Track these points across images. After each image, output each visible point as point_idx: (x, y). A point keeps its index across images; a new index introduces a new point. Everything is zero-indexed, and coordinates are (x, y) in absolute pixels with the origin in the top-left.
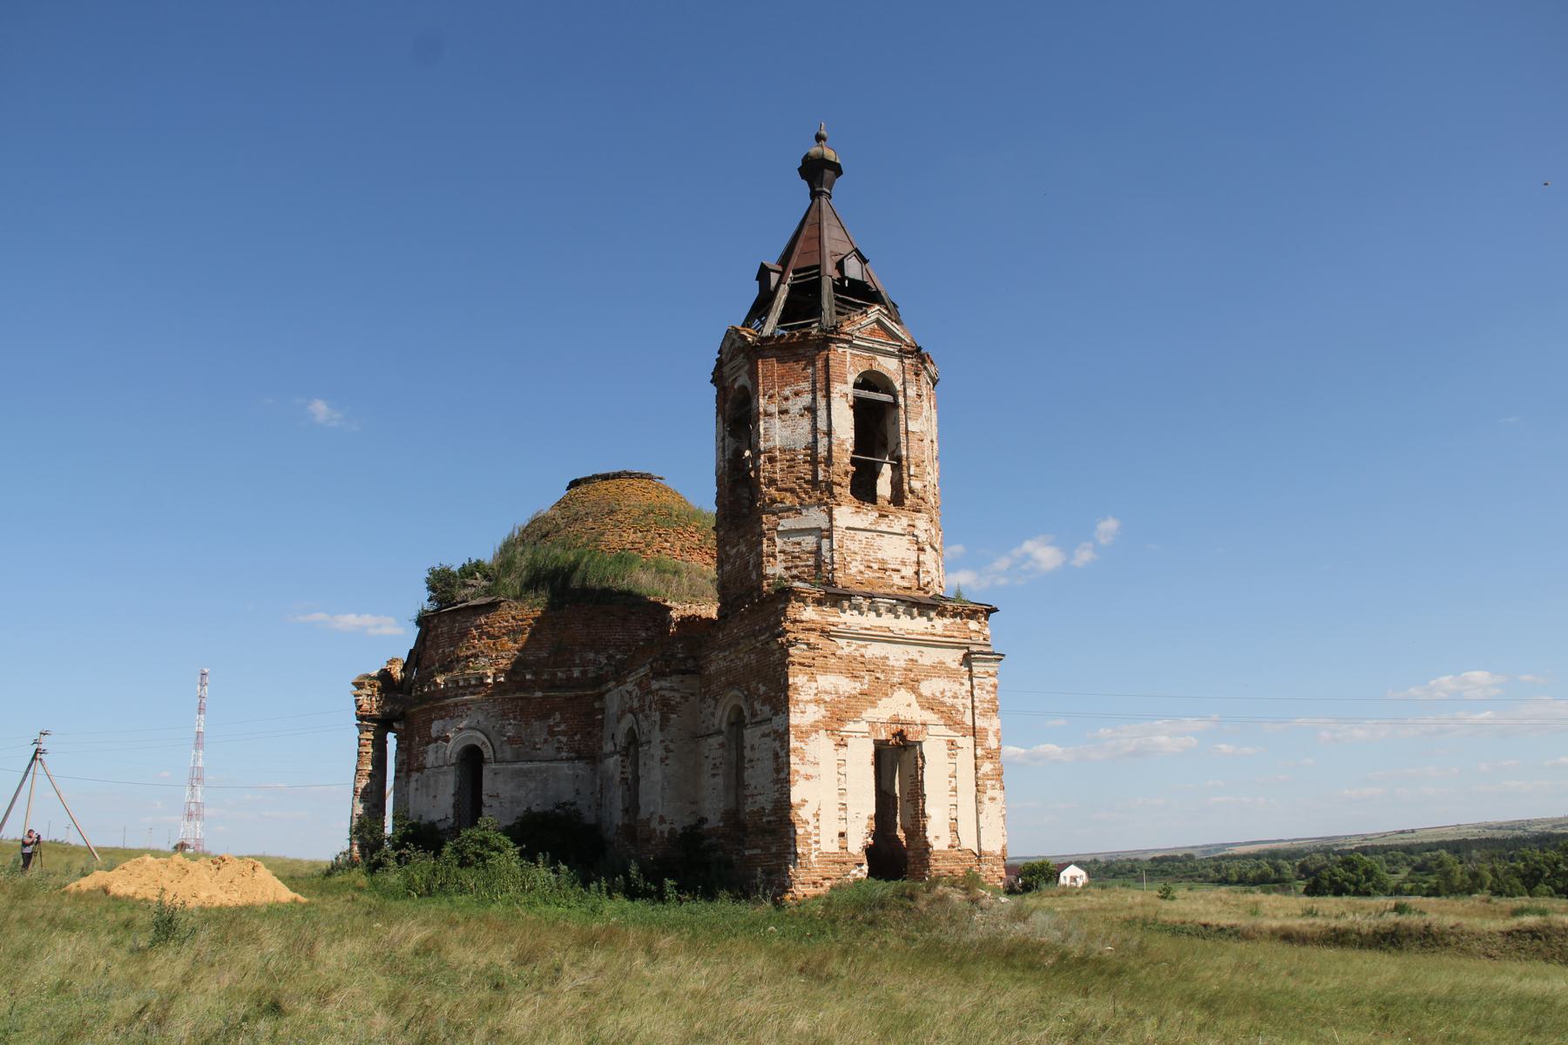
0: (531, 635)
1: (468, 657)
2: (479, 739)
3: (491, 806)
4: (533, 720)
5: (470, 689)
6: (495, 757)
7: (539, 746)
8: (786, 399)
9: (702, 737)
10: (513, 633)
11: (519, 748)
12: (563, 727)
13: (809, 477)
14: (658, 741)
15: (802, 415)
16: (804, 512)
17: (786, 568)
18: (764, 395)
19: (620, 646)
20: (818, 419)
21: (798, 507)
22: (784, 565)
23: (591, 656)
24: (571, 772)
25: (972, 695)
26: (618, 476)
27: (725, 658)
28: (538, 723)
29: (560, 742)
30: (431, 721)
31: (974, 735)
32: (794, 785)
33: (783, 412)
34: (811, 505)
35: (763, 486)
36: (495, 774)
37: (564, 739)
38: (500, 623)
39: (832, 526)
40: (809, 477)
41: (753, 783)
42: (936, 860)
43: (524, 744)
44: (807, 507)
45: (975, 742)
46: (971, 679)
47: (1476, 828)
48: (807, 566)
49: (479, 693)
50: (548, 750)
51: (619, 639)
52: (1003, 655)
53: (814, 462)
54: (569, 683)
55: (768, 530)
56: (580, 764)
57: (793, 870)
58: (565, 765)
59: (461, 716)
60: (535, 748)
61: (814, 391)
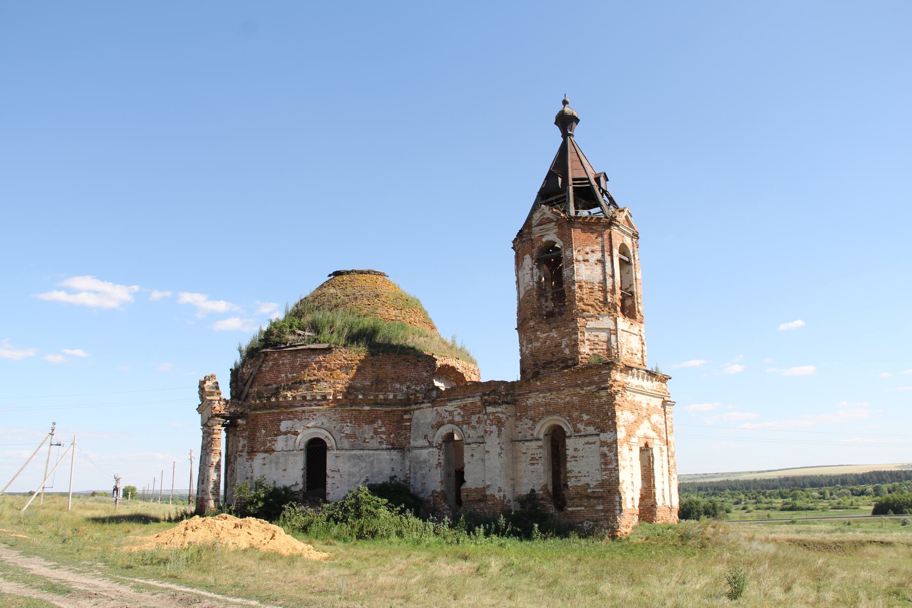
0: (359, 370)
1: (311, 381)
2: (322, 434)
3: (334, 477)
4: (363, 424)
5: (315, 402)
6: (337, 446)
7: (367, 440)
8: (587, 253)
9: (520, 441)
10: (345, 368)
11: (354, 441)
12: (383, 429)
13: (601, 299)
14: (497, 443)
15: (596, 264)
16: (601, 319)
18: (575, 250)
19: (413, 381)
20: (606, 267)
21: (598, 316)
22: (589, 347)
23: (398, 386)
24: (388, 457)
25: (666, 423)
26: (369, 272)
27: (544, 397)
28: (367, 426)
29: (381, 438)
30: (281, 421)
31: (667, 445)
33: (586, 261)
34: (605, 315)
35: (576, 301)
36: (337, 457)
37: (384, 437)
38: (334, 361)
39: (616, 329)
40: (601, 299)
41: (576, 470)
42: (658, 511)
43: (358, 438)
44: (603, 316)
45: (668, 448)
46: (665, 415)
48: (602, 349)
49: (322, 405)
50: (374, 443)
51: (412, 376)
52: (675, 402)
53: (604, 290)
54: (386, 402)
55: (580, 327)
56: (394, 452)
57: (619, 519)
58: (385, 453)
59: (308, 419)
60: (364, 442)
61: (603, 251)
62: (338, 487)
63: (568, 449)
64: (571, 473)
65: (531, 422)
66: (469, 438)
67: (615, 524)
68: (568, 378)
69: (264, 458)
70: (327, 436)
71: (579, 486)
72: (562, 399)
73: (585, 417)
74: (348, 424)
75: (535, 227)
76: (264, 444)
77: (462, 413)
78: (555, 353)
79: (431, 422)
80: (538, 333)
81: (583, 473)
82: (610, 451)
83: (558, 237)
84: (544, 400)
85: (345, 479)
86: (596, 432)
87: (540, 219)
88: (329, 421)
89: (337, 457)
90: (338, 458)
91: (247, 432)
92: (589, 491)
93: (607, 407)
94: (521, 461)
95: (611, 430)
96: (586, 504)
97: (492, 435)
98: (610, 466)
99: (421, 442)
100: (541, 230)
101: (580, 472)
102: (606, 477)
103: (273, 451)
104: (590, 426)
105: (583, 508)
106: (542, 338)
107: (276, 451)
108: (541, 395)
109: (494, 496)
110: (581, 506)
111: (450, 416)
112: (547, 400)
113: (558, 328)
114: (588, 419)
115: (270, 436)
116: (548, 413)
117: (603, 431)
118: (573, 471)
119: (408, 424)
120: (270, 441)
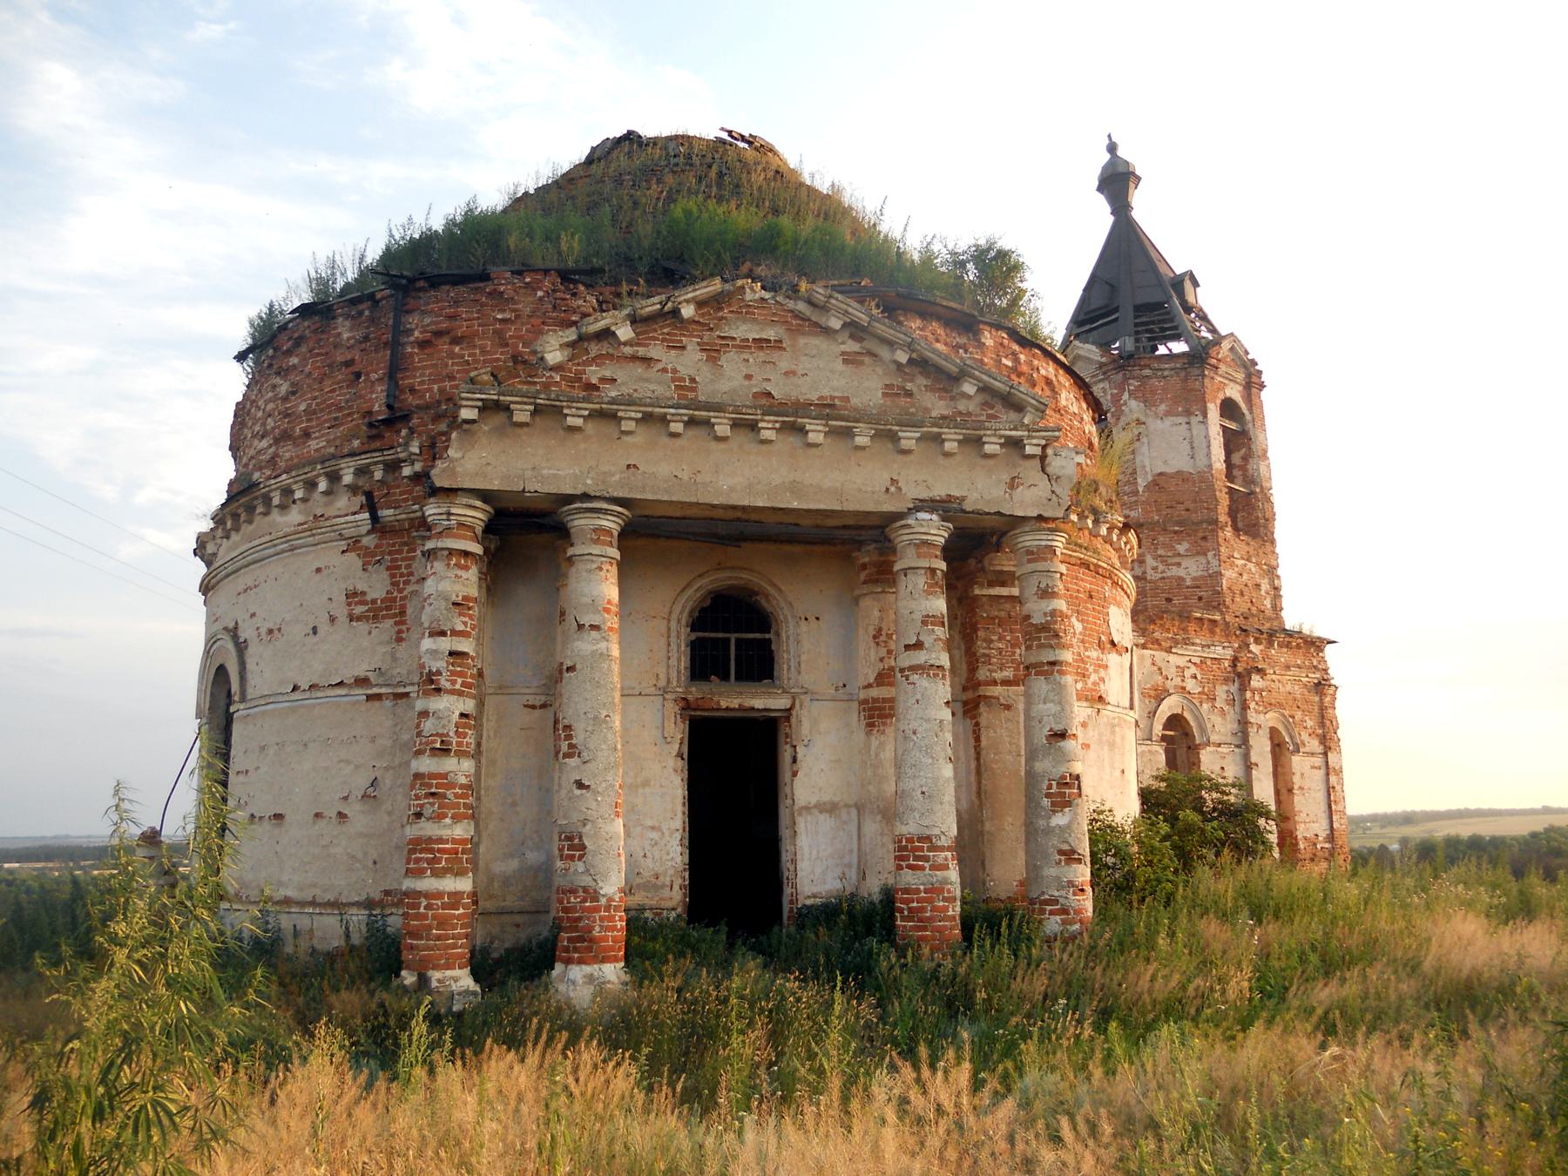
41: (1305, 810)
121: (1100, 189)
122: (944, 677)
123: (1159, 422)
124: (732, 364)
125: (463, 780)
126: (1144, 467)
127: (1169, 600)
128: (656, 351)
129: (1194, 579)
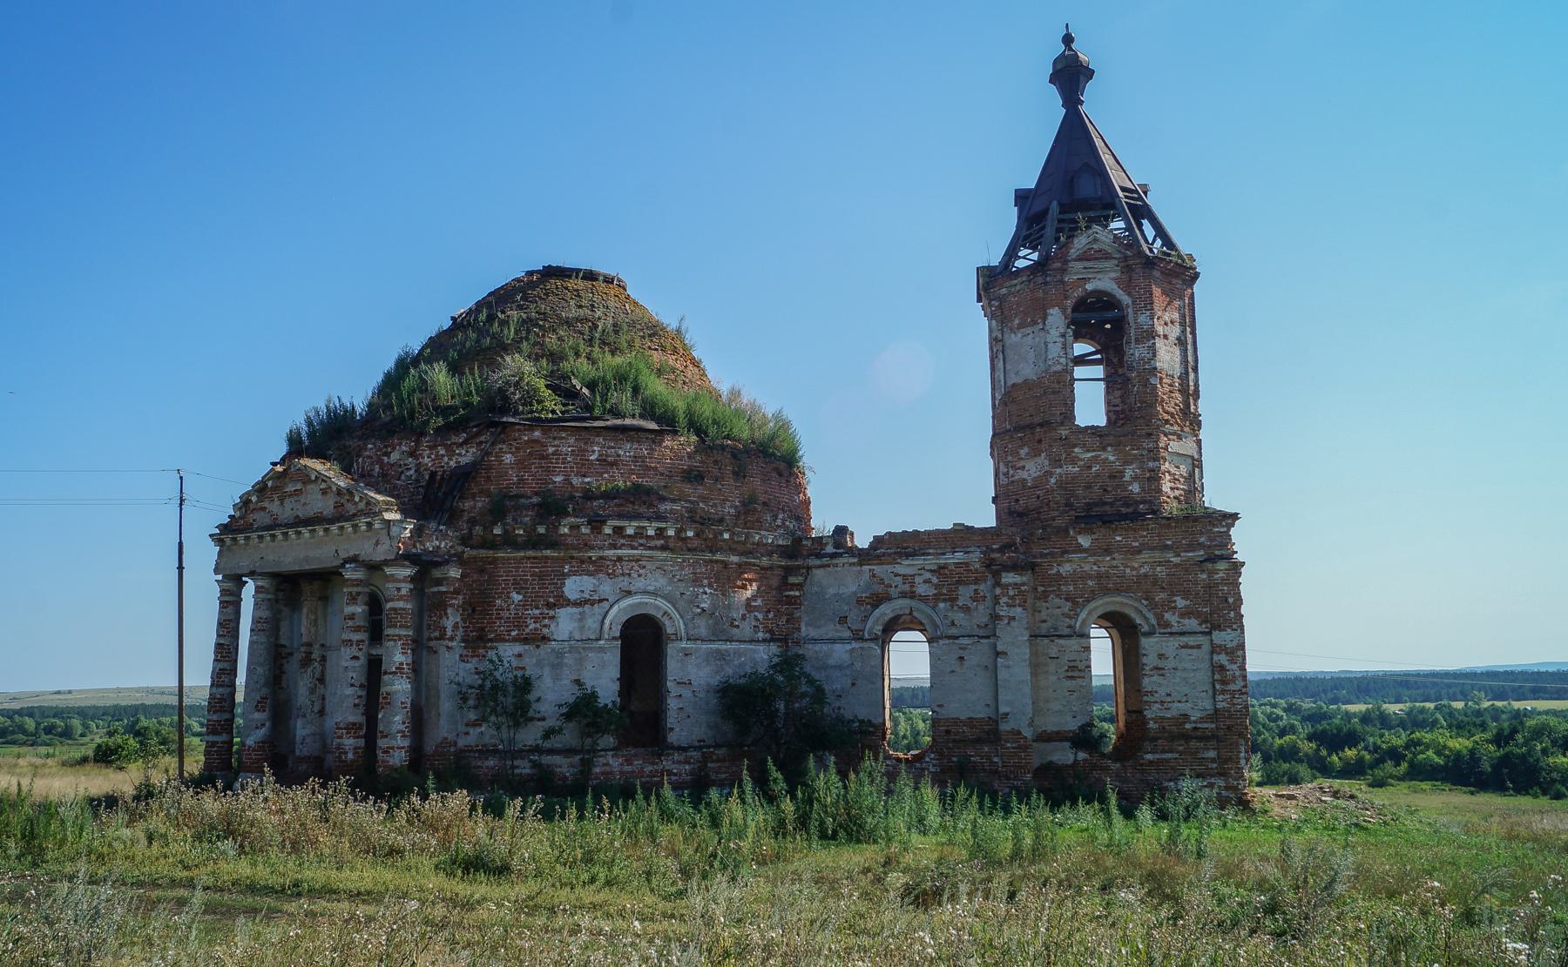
2: (657, 608)
3: (680, 695)
5: (641, 541)
17: (1172, 489)
30: (564, 576)
32: (553, 635)
36: (686, 655)
47: (137, 692)
58: (761, 648)
59: (629, 575)
60: (732, 625)
62: (689, 717)
63: (1145, 655)
64: (1152, 695)
65: (1069, 604)
66: (953, 628)
67: (1241, 782)
68: (1145, 533)
69: (520, 655)
70: (666, 613)
71: (1169, 719)
72: (1133, 569)
73: (1180, 602)
74: (706, 589)
75: (1075, 260)
76: (519, 622)
77: (935, 580)
78: (1109, 489)
79: (855, 593)
80: (1076, 450)
81: (1175, 696)
82: (1232, 662)
83: (1119, 287)
84: (1095, 568)
85: (701, 698)
86: (1203, 628)
87: (1085, 249)
88: (671, 581)
89: (686, 655)
90: (689, 657)
91: (461, 597)
92: (1188, 726)
93: (1225, 588)
94: (1047, 672)
95: (1235, 626)
96: (1181, 748)
97: (1013, 624)
98: (1232, 687)
99: (830, 630)
100: (1085, 268)
101: (1169, 695)
102: (1225, 704)
103: (545, 639)
104: (1190, 618)
105: (1177, 756)
106: (1082, 460)
107: (555, 640)
108: (1091, 559)
109: (1019, 733)
110: (1172, 752)
111: (904, 583)
112: (1103, 569)
113: (1119, 446)
114: (1186, 607)
115: (537, 608)
116: (1106, 591)
117: (1218, 627)
118: (1156, 692)
119: (797, 593)
120: (536, 619)
121: (1093, 72)
122: (351, 645)
123: (1013, 335)
124: (288, 503)
125: (219, 696)
126: (1000, 381)
127: (1017, 501)
128: (266, 504)
129: (1034, 479)
